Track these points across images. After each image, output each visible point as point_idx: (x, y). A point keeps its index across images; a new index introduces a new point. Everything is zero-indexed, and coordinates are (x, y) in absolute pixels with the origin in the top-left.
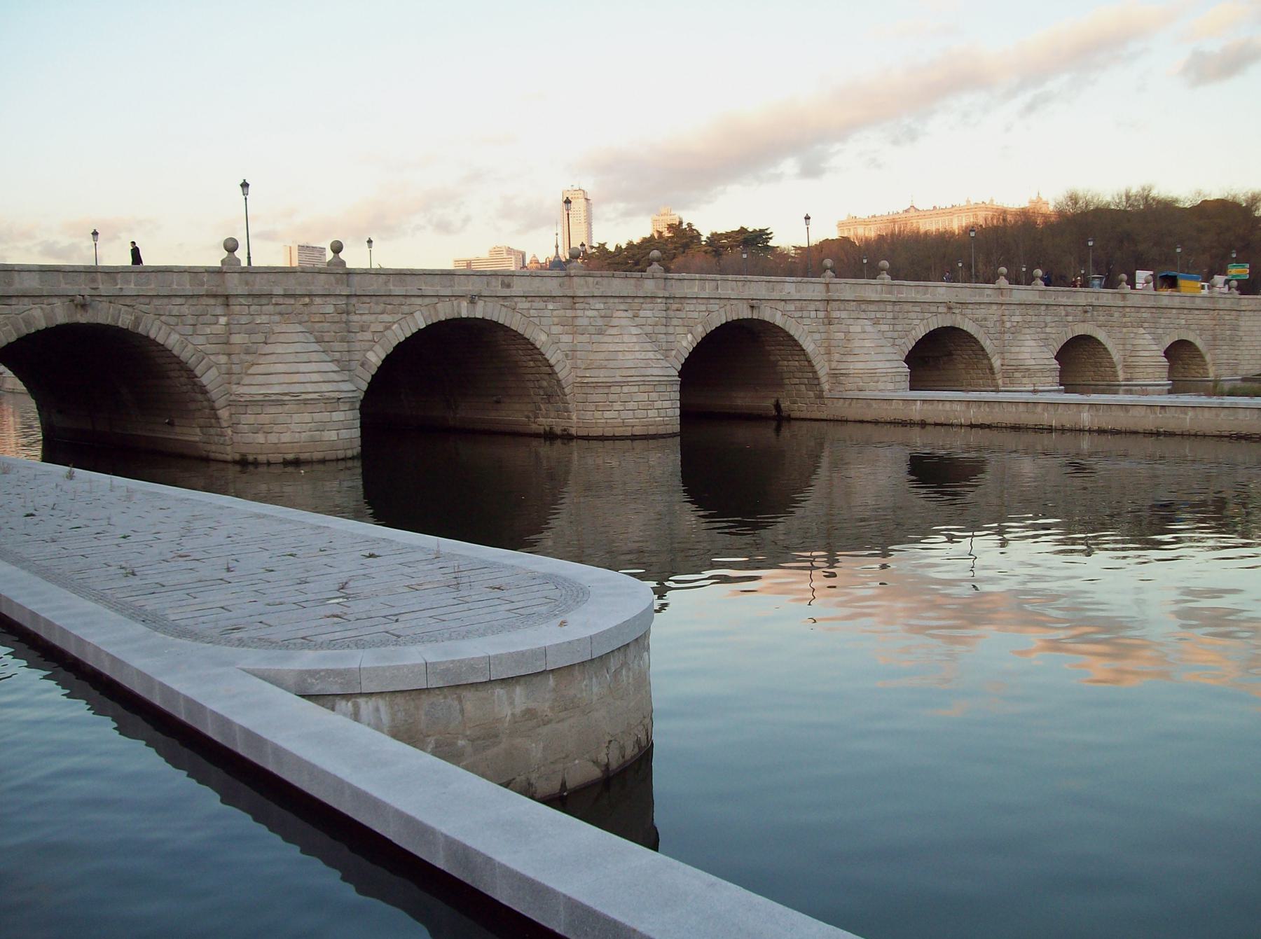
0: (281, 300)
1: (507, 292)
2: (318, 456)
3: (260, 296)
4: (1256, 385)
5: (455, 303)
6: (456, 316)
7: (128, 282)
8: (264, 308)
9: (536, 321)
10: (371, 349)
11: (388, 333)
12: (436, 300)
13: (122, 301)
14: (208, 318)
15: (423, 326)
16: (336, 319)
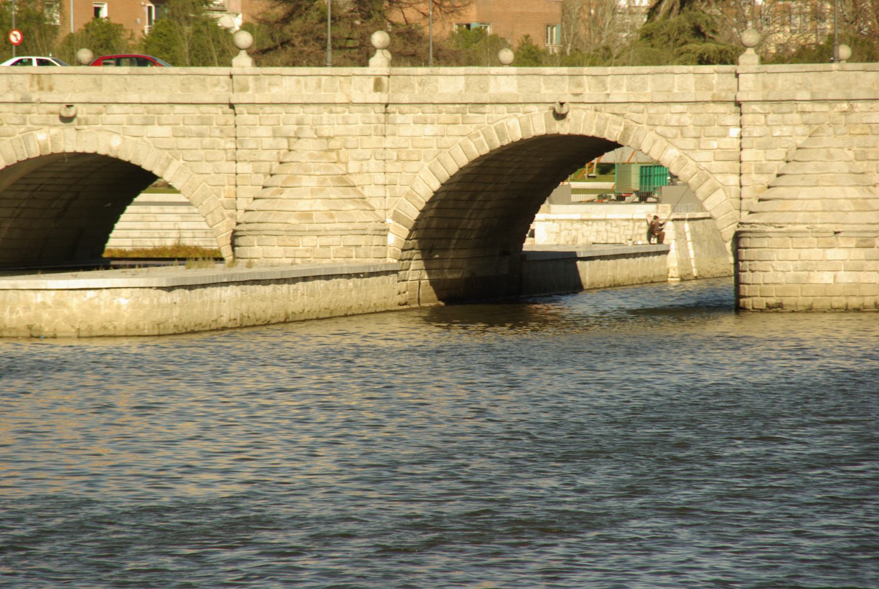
0: (808, 107)
2: (803, 301)
4: (4, 483)
7: (618, 86)
8: (788, 117)
13: (609, 108)
14: (715, 129)
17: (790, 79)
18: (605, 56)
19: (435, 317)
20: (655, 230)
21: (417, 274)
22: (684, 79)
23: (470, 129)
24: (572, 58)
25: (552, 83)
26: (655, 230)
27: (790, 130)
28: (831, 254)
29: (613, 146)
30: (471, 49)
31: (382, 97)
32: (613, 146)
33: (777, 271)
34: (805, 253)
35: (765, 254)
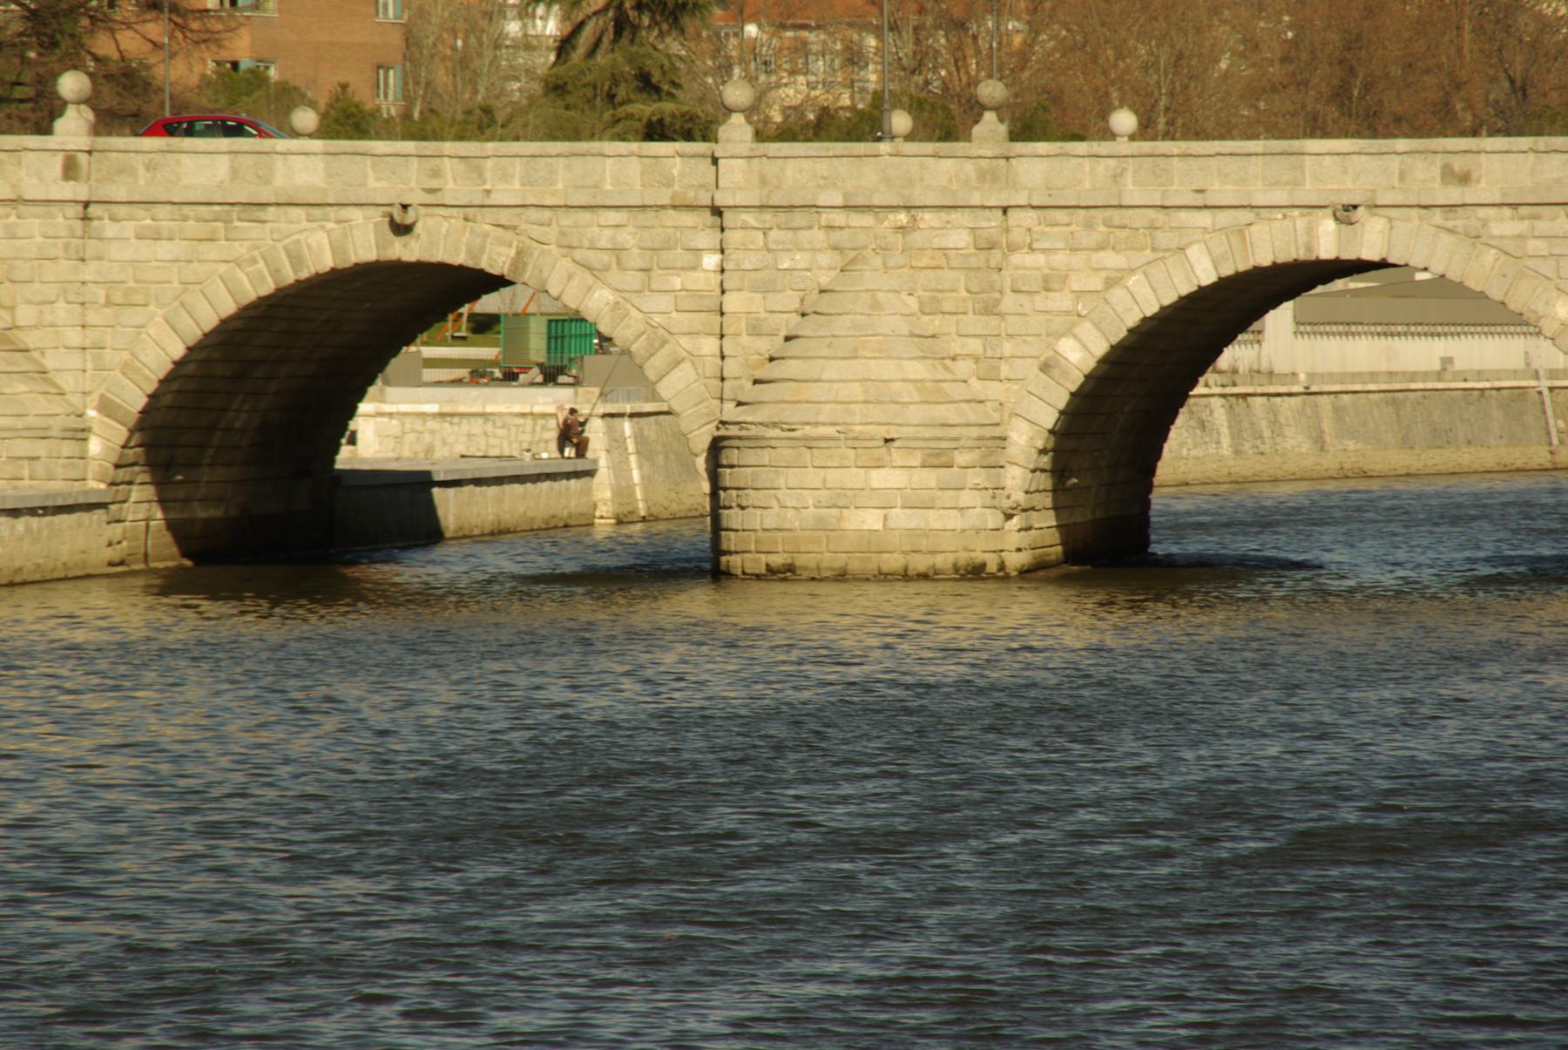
0: (839, 218)
1: (1454, 194)
3: (791, 208)
5: (1301, 224)
6: (1302, 255)
7: (506, 177)
8: (804, 236)
9: (1547, 268)
10: (1068, 331)
11: (1117, 294)
12: (1245, 216)
13: (490, 215)
14: (678, 256)
15: (1208, 277)
16: (973, 262)
17: (808, 168)
18: (483, 123)
19: (170, 585)
20: (571, 434)
21: (142, 510)
22: (621, 166)
23: (240, 249)
24: (421, 125)
25: (388, 170)
26: (571, 434)
27: (807, 258)
28: (878, 478)
29: (496, 283)
30: (234, 109)
31: (80, 191)
32: (496, 283)
33: (785, 507)
34: (834, 477)
35: (765, 478)
